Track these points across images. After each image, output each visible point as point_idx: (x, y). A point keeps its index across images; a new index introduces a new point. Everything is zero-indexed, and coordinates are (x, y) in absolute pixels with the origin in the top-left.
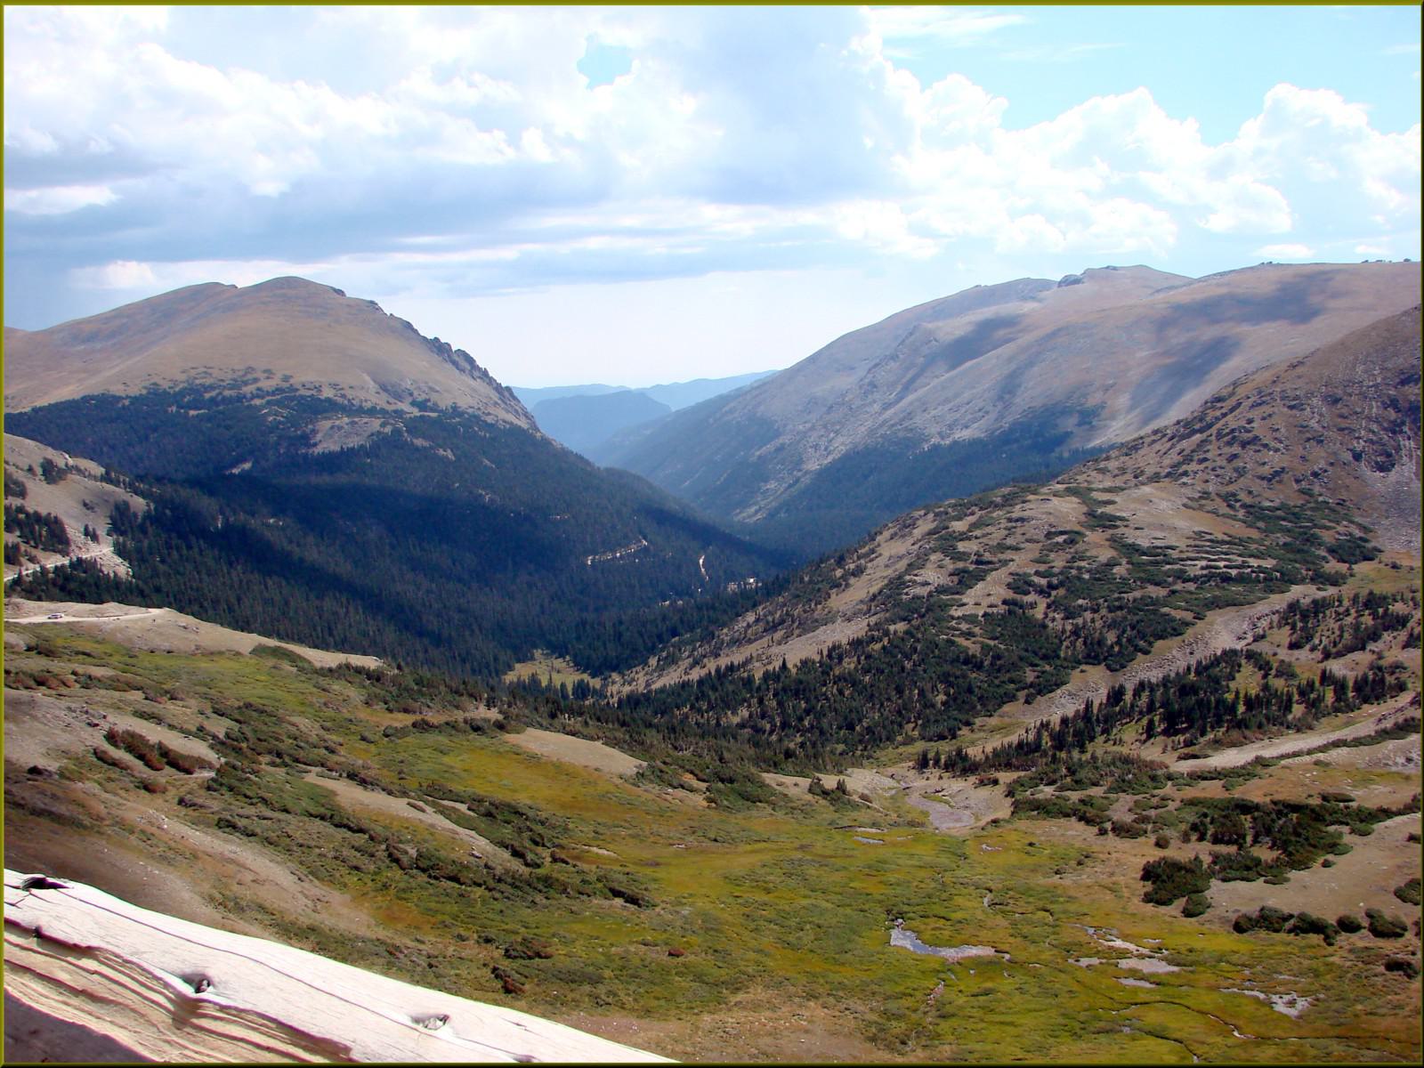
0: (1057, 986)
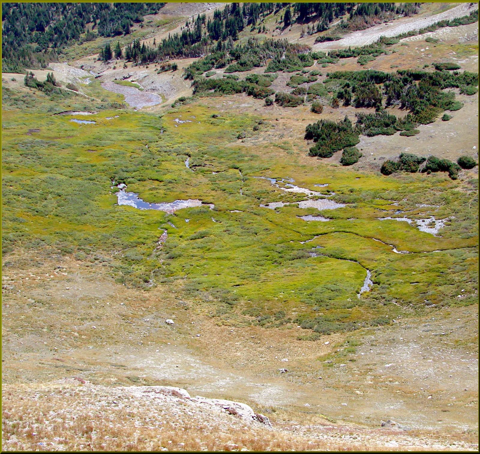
0: (255, 225)
